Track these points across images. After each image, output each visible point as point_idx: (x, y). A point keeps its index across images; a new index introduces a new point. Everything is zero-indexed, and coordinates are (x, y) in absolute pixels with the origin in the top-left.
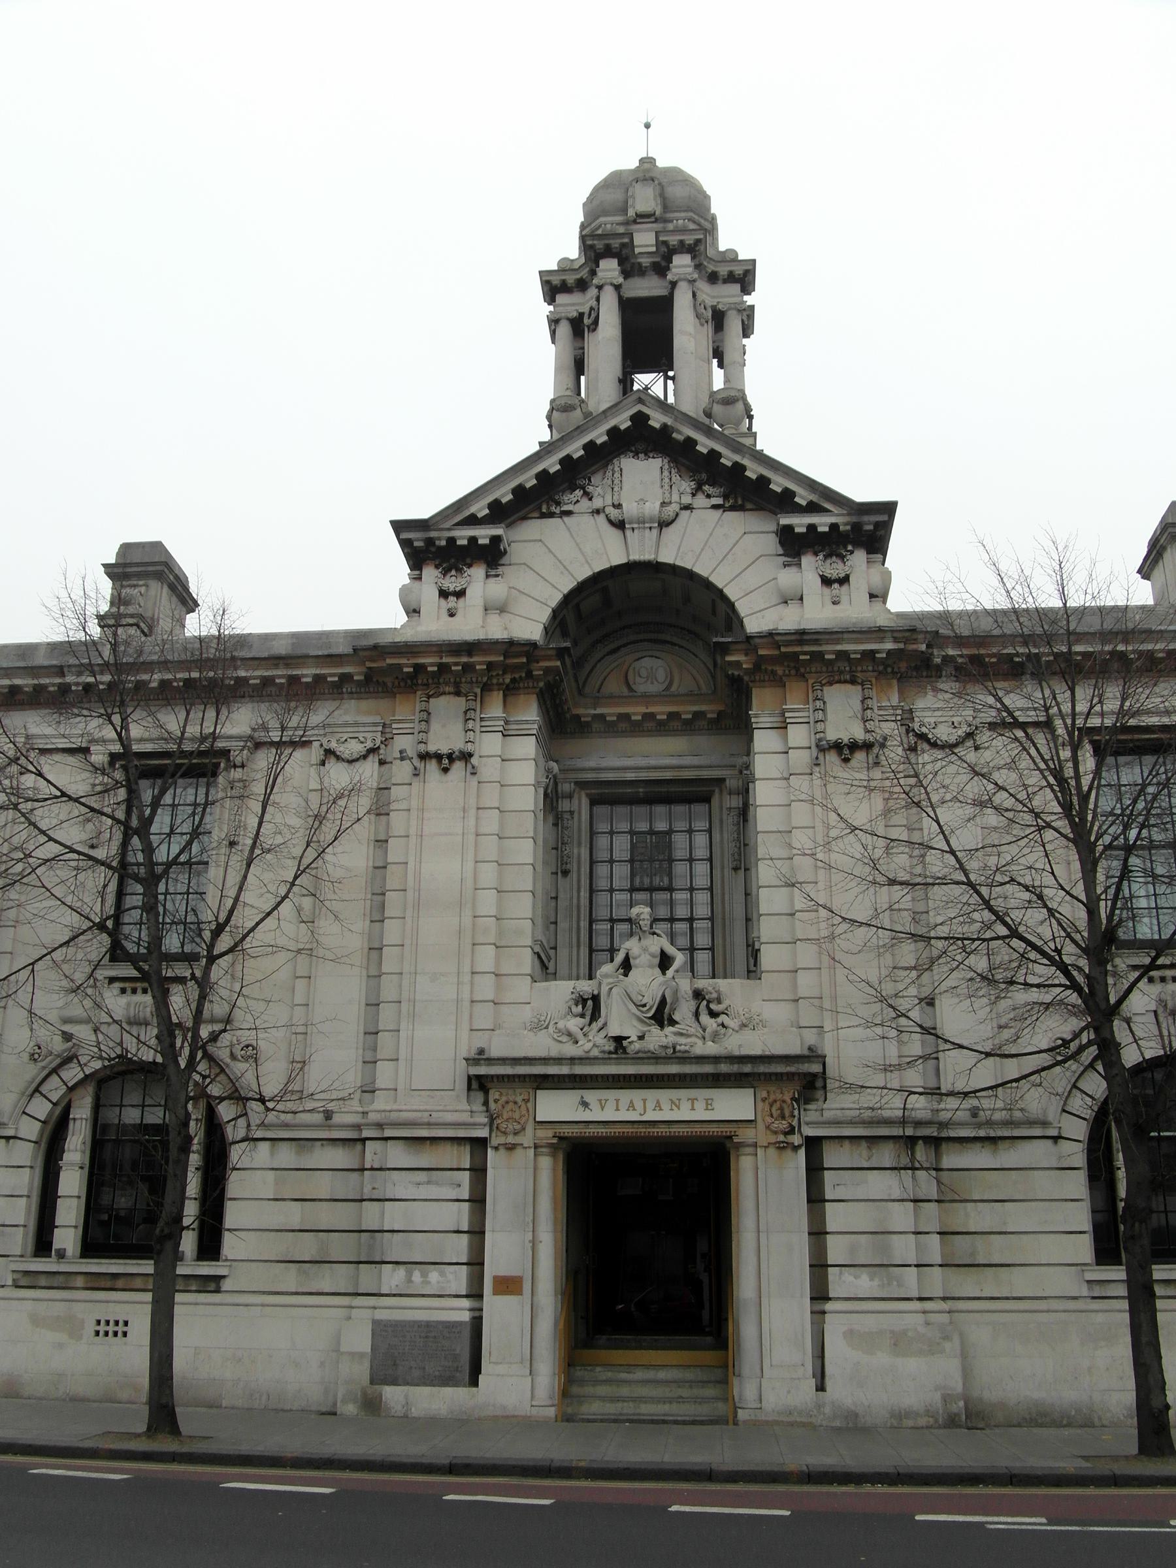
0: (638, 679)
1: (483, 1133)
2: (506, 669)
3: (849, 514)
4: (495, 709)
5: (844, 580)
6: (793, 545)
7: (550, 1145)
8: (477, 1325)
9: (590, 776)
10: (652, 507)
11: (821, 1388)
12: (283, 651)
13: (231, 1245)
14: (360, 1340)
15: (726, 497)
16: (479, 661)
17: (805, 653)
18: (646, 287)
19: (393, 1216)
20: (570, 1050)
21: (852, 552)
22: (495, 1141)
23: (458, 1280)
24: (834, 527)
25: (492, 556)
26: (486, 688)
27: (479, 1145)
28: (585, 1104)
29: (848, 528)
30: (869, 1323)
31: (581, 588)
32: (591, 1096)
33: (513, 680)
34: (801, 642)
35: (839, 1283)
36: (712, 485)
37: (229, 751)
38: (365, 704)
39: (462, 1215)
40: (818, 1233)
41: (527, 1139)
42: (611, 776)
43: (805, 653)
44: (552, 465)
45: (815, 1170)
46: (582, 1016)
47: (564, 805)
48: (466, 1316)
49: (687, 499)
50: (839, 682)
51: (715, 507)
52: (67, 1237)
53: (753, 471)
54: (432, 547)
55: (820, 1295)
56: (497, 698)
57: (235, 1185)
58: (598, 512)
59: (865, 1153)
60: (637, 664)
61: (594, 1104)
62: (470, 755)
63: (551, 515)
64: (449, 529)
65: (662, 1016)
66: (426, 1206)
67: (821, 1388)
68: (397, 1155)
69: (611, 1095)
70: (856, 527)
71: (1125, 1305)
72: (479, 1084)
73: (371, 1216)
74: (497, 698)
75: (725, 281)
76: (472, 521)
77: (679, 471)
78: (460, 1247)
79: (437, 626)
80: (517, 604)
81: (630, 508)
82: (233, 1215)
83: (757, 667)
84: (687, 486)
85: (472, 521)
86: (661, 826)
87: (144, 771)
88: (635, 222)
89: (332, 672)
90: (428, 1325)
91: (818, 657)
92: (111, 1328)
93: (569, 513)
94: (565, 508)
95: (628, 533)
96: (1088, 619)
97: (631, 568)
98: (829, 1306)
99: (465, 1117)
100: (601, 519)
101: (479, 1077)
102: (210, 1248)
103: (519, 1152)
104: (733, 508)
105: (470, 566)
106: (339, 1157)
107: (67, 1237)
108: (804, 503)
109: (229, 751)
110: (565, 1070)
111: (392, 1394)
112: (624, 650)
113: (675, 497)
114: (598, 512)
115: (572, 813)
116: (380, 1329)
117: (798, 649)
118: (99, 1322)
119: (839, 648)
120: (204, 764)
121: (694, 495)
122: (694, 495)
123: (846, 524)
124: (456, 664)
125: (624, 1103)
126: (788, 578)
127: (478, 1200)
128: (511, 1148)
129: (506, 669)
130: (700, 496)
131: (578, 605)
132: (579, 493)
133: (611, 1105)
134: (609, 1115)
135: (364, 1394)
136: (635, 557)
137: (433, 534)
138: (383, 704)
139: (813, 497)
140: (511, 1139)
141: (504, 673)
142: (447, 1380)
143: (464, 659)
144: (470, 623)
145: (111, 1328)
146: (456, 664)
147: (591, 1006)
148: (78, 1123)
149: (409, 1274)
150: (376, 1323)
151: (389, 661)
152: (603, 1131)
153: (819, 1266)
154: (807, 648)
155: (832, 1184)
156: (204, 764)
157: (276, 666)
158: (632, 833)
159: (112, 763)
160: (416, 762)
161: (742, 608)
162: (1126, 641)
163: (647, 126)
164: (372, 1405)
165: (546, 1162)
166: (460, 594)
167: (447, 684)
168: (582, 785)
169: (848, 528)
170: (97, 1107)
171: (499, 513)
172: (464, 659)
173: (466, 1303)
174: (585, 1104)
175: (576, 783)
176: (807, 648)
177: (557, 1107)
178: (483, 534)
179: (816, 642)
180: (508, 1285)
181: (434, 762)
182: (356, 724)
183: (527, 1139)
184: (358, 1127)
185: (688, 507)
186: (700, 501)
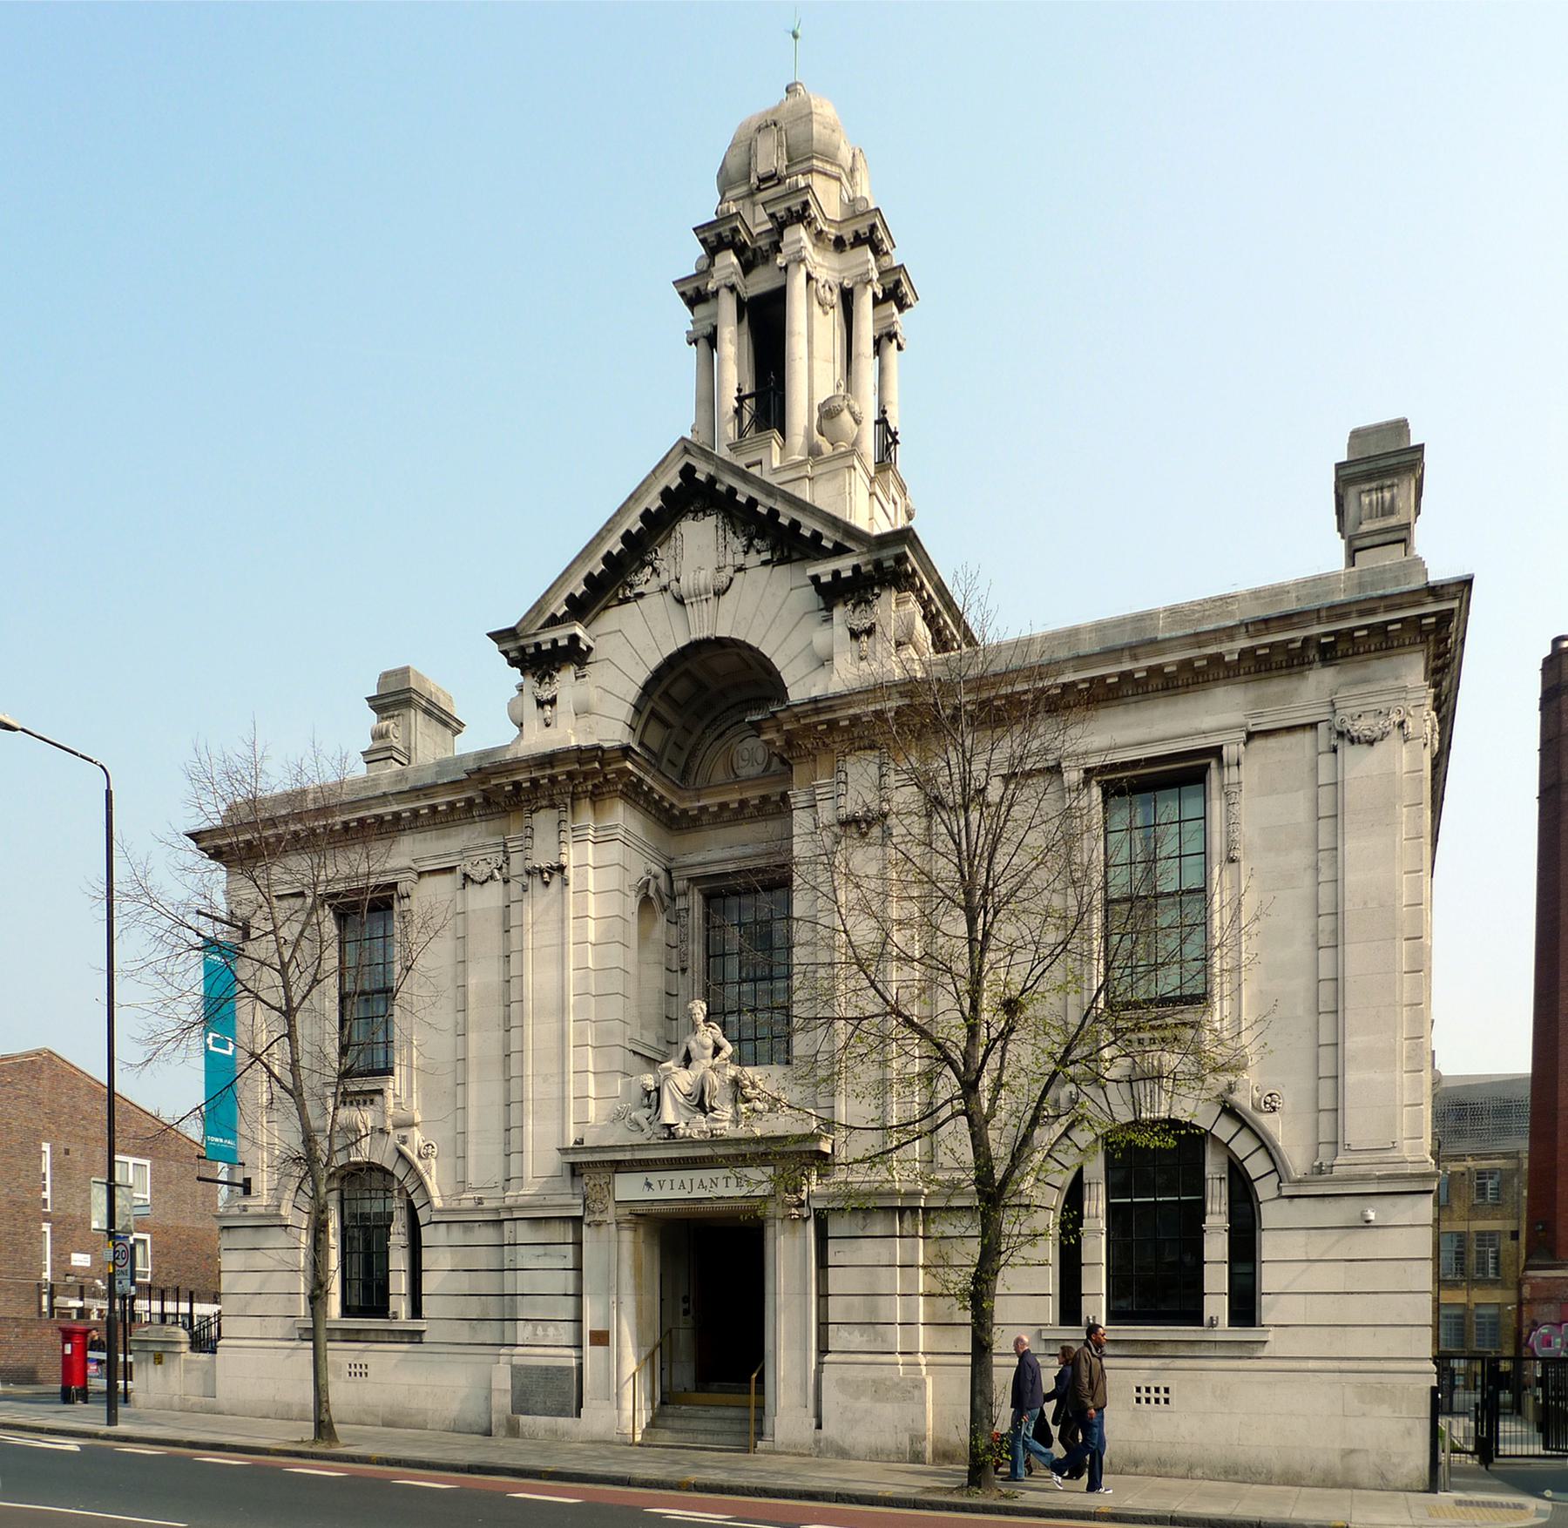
0: (742, 763)
1: (579, 1213)
2: (587, 776)
3: (869, 551)
4: (586, 816)
5: (552, 702)
6: (832, 593)
7: (629, 1221)
8: (580, 1367)
9: (698, 871)
10: (706, 578)
11: (819, 1426)
12: (428, 779)
13: (1269, 1309)
14: (502, 1379)
15: (773, 549)
16: (559, 771)
17: (822, 723)
18: (760, 283)
19: (523, 1283)
20: (638, 1138)
21: (878, 596)
22: (587, 1220)
23: (566, 1333)
24: (856, 568)
25: (575, 655)
26: (575, 797)
27: (578, 1221)
28: (649, 1185)
29: (870, 567)
30: (854, 1373)
31: (658, 676)
32: (654, 1177)
33: (595, 786)
34: (817, 711)
35: (837, 1338)
36: (762, 539)
37: (1221, 747)
38: (481, 827)
39: (567, 1281)
40: (823, 1295)
41: (610, 1216)
42: (715, 869)
43: (822, 723)
44: (614, 545)
45: (822, 1239)
46: (650, 1107)
47: (681, 903)
48: (574, 1362)
49: (740, 559)
50: (860, 749)
51: (765, 563)
52: (1096, 1306)
53: (786, 516)
54: (539, 655)
55: (823, 1350)
56: (585, 804)
57: (1269, 1246)
58: (665, 589)
59: (861, 1222)
60: (740, 747)
61: (656, 1186)
62: (885, 816)
63: (626, 600)
64: (535, 635)
65: (700, 1104)
66: (541, 1272)
67: (819, 1426)
68: (524, 1233)
69: (666, 1176)
70: (878, 564)
71: (969, 1360)
72: (575, 1170)
73: (511, 1282)
74: (585, 804)
75: (853, 246)
76: (554, 621)
77: (733, 525)
78: (566, 1308)
79: (538, 740)
80: (597, 708)
81: (686, 585)
82: (1270, 1278)
83: (789, 744)
84: (738, 543)
85: (554, 621)
86: (763, 915)
87: (1132, 783)
88: (758, 189)
89: (458, 797)
90: (547, 1368)
91: (832, 725)
92: (1153, 1394)
93: (641, 595)
94: (638, 590)
95: (689, 607)
96: (1005, 655)
97: (696, 647)
98: (828, 1358)
99: (568, 1200)
100: (668, 595)
101: (573, 1164)
102: (1244, 1309)
103: (604, 1228)
104: (781, 562)
105: (558, 671)
106: (488, 1235)
107: (1096, 1306)
108: (830, 545)
109: (1221, 747)
110: (627, 1156)
111: (523, 1419)
112: (729, 733)
113: (729, 560)
114: (665, 589)
115: (687, 910)
116: (517, 1371)
117: (815, 719)
118: (1138, 1390)
119: (851, 711)
120: (1187, 773)
121: (746, 553)
122: (746, 553)
123: (866, 564)
124: (543, 777)
125: (677, 1184)
126: (820, 637)
127: (578, 1269)
128: (599, 1224)
129: (587, 776)
130: (753, 553)
131: (666, 693)
132: (648, 570)
133: (667, 1185)
134: (666, 1194)
135: (508, 1420)
136: (697, 635)
137: (523, 642)
138: (495, 825)
139: (838, 537)
140: (598, 1217)
141: (585, 780)
142: (561, 1413)
143: (548, 772)
144: (568, 734)
145: (1153, 1394)
146: (543, 777)
147: (653, 1098)
148: (1094, 1187)
149: (535, 1329)
150: (513, 1367)
151: (493, 782)
152: (664, 1207)
153: (823, 1324)
154: (823, 717)
155: (835, 1253)
156: (1187, 773)
157: (418, 798)
158: (740, 925)
159: (1086, 782)
160: (836, 829)
161: (787, 679)
162: (1135, 658)
163: (795, 36)
164: (513, 1430)
165: (627, 1236)
166: (552, 702)
167: (543, 797)
168: (693, 880)
169: (870, 567)
170: (342, 1201)
171: (580, 608)
172: (548, 772)
173: (572, 1352)
174: (649, 1185)
175: (689, 880)
176: (823, 717)
177: (629, 1187)
178: (561, 634)
179: (831, 709)
180: (600, 1338)
181: (854, 829)
182: (483, 846)
183: (610, 1216)
184: (497, 1210)
185: (740, 569)
186: (753, 559)
